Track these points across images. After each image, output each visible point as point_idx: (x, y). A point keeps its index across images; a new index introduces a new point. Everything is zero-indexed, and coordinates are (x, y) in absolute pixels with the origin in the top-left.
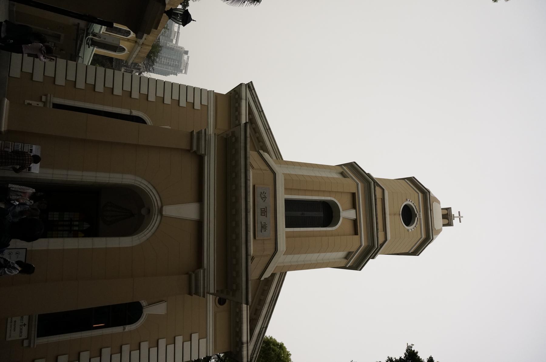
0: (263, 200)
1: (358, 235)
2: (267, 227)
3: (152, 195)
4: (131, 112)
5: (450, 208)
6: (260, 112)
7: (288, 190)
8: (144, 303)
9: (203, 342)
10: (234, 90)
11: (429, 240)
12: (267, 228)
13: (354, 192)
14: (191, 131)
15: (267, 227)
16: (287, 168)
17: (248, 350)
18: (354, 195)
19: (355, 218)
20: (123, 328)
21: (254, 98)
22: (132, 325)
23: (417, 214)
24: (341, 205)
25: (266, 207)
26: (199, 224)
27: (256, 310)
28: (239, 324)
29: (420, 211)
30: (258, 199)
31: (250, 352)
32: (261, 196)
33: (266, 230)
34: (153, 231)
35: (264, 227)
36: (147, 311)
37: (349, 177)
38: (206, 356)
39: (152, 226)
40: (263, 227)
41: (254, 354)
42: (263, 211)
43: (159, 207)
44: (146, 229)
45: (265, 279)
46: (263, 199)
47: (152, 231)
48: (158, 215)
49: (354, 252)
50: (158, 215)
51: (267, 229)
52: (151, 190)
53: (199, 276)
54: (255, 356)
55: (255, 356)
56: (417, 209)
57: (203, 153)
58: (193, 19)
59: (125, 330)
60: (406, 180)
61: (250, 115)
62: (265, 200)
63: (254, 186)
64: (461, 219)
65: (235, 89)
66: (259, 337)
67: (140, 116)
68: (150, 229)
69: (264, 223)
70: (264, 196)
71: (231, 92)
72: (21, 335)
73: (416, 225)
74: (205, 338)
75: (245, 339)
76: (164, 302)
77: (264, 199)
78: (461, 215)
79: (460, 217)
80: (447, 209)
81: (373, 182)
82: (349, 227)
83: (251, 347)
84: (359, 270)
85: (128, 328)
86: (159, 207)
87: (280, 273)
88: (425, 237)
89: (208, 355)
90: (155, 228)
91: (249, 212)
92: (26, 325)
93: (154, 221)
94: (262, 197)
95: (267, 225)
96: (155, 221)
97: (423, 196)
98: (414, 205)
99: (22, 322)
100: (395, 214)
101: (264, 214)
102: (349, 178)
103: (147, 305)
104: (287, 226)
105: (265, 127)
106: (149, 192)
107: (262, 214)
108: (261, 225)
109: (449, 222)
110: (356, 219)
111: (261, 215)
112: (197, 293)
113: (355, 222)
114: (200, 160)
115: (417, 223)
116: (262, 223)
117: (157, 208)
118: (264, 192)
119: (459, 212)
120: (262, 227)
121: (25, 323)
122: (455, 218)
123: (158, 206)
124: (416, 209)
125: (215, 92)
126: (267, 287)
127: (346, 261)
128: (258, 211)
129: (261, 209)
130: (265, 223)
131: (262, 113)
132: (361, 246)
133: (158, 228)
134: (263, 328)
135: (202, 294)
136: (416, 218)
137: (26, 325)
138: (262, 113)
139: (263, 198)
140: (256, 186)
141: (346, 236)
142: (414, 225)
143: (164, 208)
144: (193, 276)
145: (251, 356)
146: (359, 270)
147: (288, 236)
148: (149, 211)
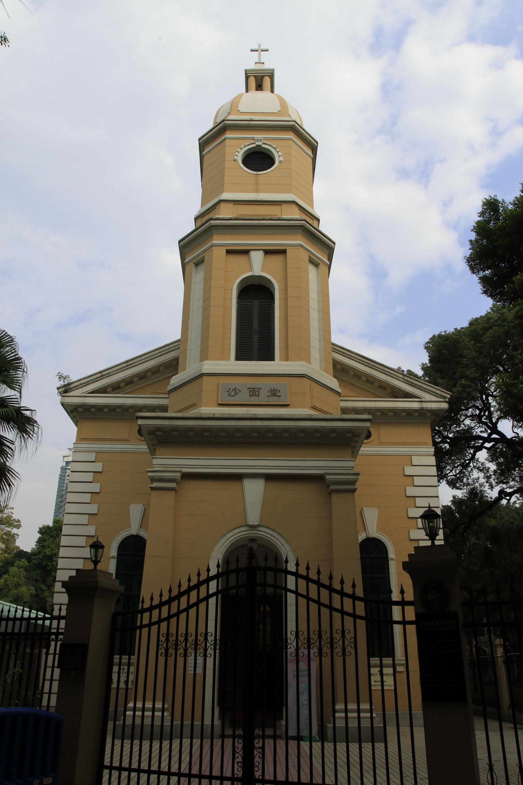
0: (238, 393)
1: (286, 250)
2: (274, 388)
3: (234, 537)
4: (113, 557)
5: (246, 71)
7: (224, 357)
8: (362, 537)
9: (415, 460)
11: (297, 128)
12: (272, 389)
15: (274, 388)
16: (191, 350)
17: (431, 402)
18: (229, 252)
20: (392, 561)
21: (81, 384)
22: (388, 551)
23: (257, 144)
24: (244, 273)
25: (248, 389)
26: (269, 478)
27: (380, 387)
28: (396, 412)
29: (253, 139)
30: (237, 400)
31: (434, 398)
32: (234, 396)
33: (278, 389)
35: (274, 393)
36: (373, 533)
38: (434, 456)
39: (272, 538)
40: (274, 394)
41: (436, 393)
44: (276, 544)
45: (340, 387)
46: (236, 393)
48: (258, 530)
49: (309, 256)
50: (258, 530)
51: (277, 389)
52: (228, 539)
54: (438, 392)
55: (438, 392)
56: (249, 143)
57: (179, 474)
58: (96, 539)
59: (395, 558)
60: (204, 153)
61: (107, 390)
62: (238, 389)
63: (221, 405)
64: (263, 48)
65: (69, 412)
66: (416, 385)
67: (117, 546)
68: (275, 540)
69: (269, 392)
70: (233, 391)
71: (72, 416)
73: (273, 147)
74: (411, 457)
75: (415, 405)
76: (362, 510)
77: (237, 391)
78: (256, 48)
79: (259, 50)
80: (247, 77)
82: (277, 260)
83: (427, 397)
84: (334, 246)
85: (391, 555)
86: (248, 529)
87: (333, 353)
88: (291, 133)
89: (433, 453)
90: (274, 534)
91: (256, 416)
92: (125, 669)
93: (265, 534)
95: (271, 389)
96: (264, 533)
97: (229, 129)
98: (244, 147)
99: (376, 675)
100: (257, 183)
101: (257, 392)
103: (365, 532)
105: (125, 368)
106: (230, 542)
107: (257, 394)
108: (272, 397)
109: (269, 76)
111: (258, 396)
112: (354, 483)
113: (268, 252)
114: (187, 476)
115: (270, 146)
116: (269, 394)
117: (249, 532)
118: (229, 392)
119: (251, 51)
120: (274, 395)
122: (262, 62)
123: (249, 530)
124: (249, 145)
125: (75, 442)
126: (350, 371)
127: (321, 266)
128: (254, 400)
129: (250, 396)
130: (269, 391)
131: (103, 373)
132: (302, 246)
134: (404, 379)
135: (355, 477)
136: (263, 146)
137: (125, 669)
138: (103, 373)
139: (235, 392)
140: (220, 402)
141: (288, 269)
142: (273, 151)
143: (250, 523)
144: (333, 487)
145: (438, 397)
146: (334, 246)
147: (286, 358)
148: (253, 540)
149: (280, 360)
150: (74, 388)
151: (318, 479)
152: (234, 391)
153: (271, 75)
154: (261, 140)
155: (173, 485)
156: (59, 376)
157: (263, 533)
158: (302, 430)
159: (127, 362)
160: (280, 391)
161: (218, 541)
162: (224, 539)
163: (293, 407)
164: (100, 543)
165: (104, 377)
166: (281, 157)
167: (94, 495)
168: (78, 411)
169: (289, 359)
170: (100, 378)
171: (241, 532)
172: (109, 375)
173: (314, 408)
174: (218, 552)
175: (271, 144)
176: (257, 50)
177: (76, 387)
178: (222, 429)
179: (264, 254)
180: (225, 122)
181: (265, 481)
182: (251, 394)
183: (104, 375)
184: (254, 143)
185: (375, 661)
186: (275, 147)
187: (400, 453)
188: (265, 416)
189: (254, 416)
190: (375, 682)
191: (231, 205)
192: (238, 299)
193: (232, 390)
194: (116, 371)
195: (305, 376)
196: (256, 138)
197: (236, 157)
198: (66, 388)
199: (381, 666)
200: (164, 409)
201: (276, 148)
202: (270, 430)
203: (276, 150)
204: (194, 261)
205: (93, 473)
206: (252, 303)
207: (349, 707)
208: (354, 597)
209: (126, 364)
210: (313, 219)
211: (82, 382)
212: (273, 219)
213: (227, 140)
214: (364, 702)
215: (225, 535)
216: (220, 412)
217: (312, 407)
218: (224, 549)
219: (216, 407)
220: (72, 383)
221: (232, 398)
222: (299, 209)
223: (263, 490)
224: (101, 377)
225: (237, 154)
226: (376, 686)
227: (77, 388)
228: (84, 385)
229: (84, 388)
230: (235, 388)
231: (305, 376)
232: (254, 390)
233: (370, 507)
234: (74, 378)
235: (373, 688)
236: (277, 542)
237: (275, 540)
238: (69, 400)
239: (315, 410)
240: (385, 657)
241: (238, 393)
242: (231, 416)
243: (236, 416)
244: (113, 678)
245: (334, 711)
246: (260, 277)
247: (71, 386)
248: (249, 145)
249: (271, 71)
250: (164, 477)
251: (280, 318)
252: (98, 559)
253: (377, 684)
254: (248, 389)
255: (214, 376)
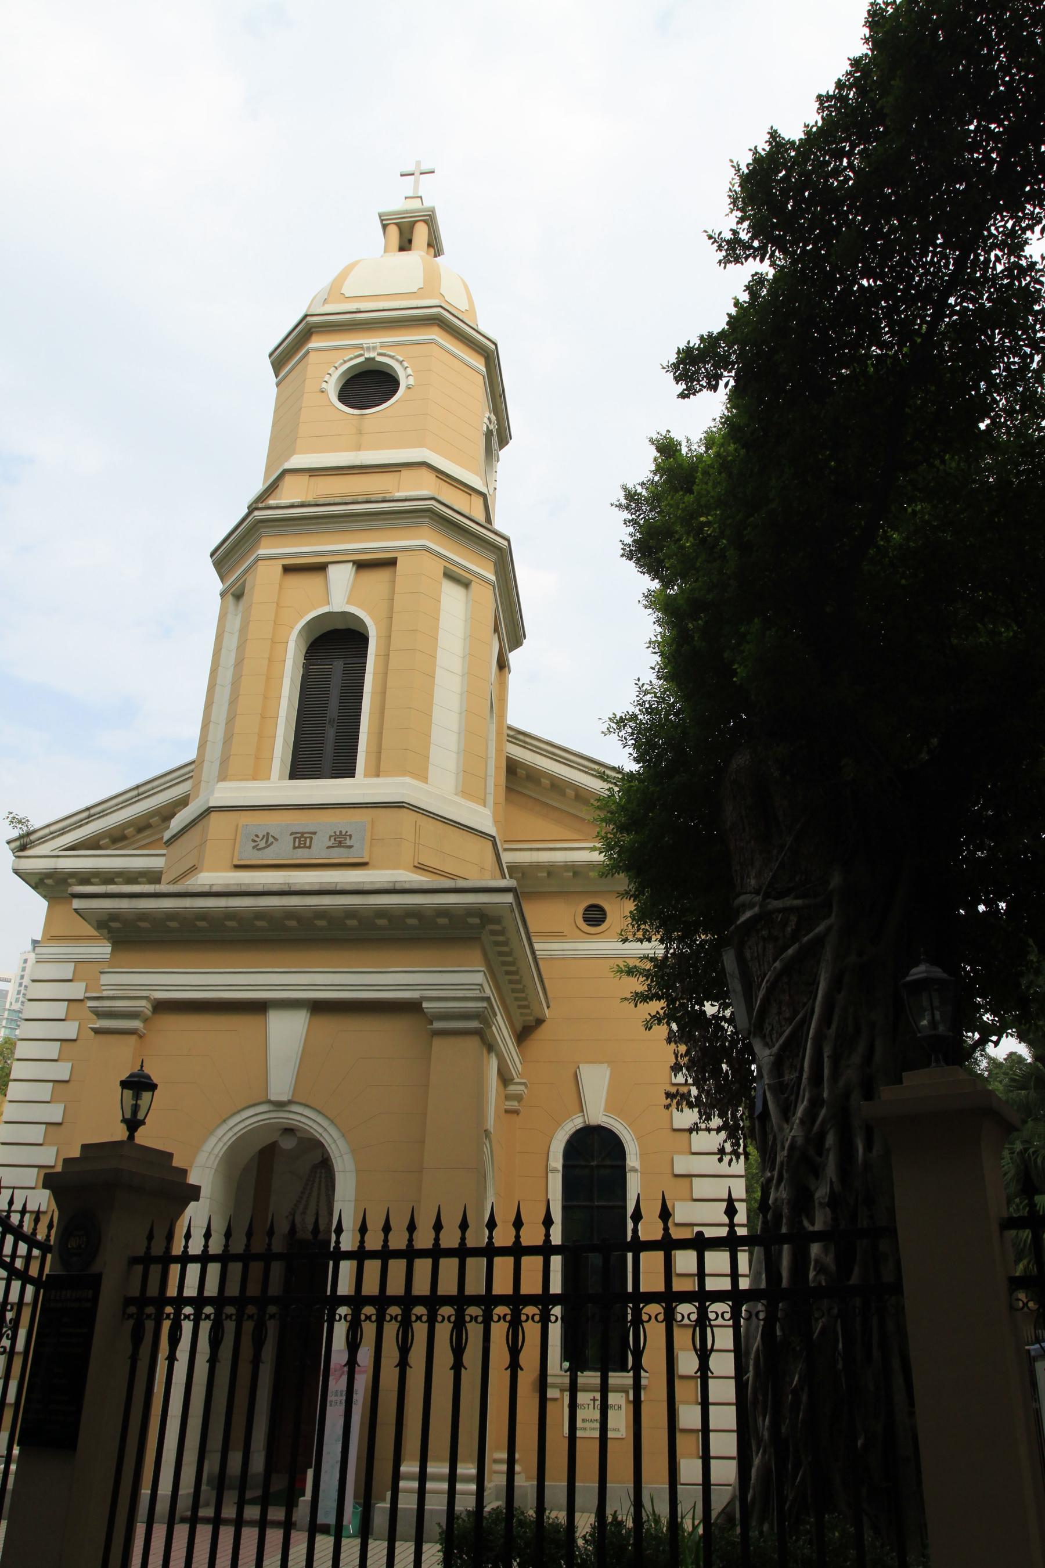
0: (272, 843)
2: (341, 832)
3: (242, 1125)
5: (379, 214)
6: (92, 816)
7: (258, 772)
10: (35, 887)
12: (344, 833)
13: (280, 569)
14: (93, 1033)
15: (341, 832)
18: (288, 569)
19: (351, 564)
21: (52, 833)
23: (367, 355)
26: (319, 1008)
29: (360, 347)
30: (269, 856)
34: (325, 1123)
35: (340, 840)
36: (597, 1115)
37: (241, 581)
39: (315, 1126)
42: (300, 843)
43: (272, 1108)
46: (269, 842)
47: (325, 1126)
50: (290, 1112)
51: (347, 832)
52: (231, 1129)
53: (443, 1010)
56: (352, 356)
63: (238, 867)
64: (424, 167)
68: (320, 1130)
69: (330, 840)
70: (262, 839)
72: (616, 1407)
73: (397, 360)
77: (271, 840)
79: (417, 173)
80: (385, 227)
81: (256, 513)
82: (378, 579)
85: (632, 1160)
88: (436, 329)
90: (319, 1119)
92: (594, 1397)
93: (303, 1119)
94: (264, 845)
95: (335, 832)
97: (317, 332)
98: (341, 364)
99: (586, 1406)
100: (360, 432)
101: (308, 840)
102: (245, 581)
103: (582, 1114)
104: (350, 773)
109: (425, 221)
110: (354, 562)
111: (310, 847)
113: (361, 566)
114: (163, 1007)
115: (392, 357)
116: (330, 844)
118: (254, 841)
119: (402, 175)
120: (340, 844)
121: (591, 1400)
123: (270, 1111)
124: (351, 359)
128: (302, 856)
129: (295, 848)
130: (331, 837)
131: (93, 811)
133: (319, 1112)
136: (379, 359)
137: (594, 1397)
138: (93, 811)
139: (267, 841)
141: (395, 595)
143: (273, 1098)
144: (438, 1025)
147: (376, 771)
149: (365, 776)
150: (38, 840)
151: (410, 1008)
152: (265, 838)
153: (430, 220)
154: (374, 348)
155: (136, 1024)
156: (9, 819)
157: (298, 1118)
158: (382, 912)
159: (137, 787)
160: (353, 837)
161: (212, 1133)
162: (225, 1127)
163: (375, 868)
164: (148, 1077)
165: (93, 818)
166: (409, 377)
167: (65, 1044)
168: (45, 884)
169: (381, 773)
170: (87, 820)
171: (256, 1115)
172: (102, 814)
173: (420, 868)
174: (210, 1153)
175: (392, 354)
176: (412, 172)
177: (42, 838)
178: (231, 915)
179: (354, 568)
180: (309, 319)
181: (309, 1014)
182: (297, 845)
183: (95, 815)
184: (361, 355)
185: (590, 1378)
186: (401, 359)
187: (82, 956)
188: (307, 888)
189: (286, 888)
190: (584, 1421)
191: (304, 478)
192: (305, 659)
193: (261, 837)
194: (116, 805)
195: (404, 804)
196: (365, 346)
197: (324, 385)
198: (22, 842)
199: (604, 1389)
200: (153, 876)
201: (403, 361)
202: (321, 914)
203: (403, 366)
204: (231, 592)
205: (67, 1003)
206: (331, 665)
207: (430, 1470)
208: (32, 1242)
209: (135, 793)
210: (470, 495)
211: (53, 828)
212: (373, 500)
213: (311, 354)
214: (439, 1459)
215: (224, 1121)
216: (221, 882)
217: (415, 866)
218: (223, 1147)
219: (228, 871)
220: (35, 831)
221: (260, 852)
222: (437, 476)
223: (305, 1031)
224: (89, 818)
225: (327, 378)
226: (585, 1429)
227: (43, 840)
228: (56, 834)
229: (57, 840)
230: (268, 834)
231: (404, 804)
232: (302, 836)
233: (596, 1062)
234: (36, 823)
235: (579, 1434)
236: (325, 1135)
237: (320, 1130)
238: (29, 865)
239: (424, 872)
240: (615, 1371)
241: (272, 843)
242: (244, 889)
243: (252, 889)
244: (568, 1410)
245: (396, 1476)
246: (344, 614)
247: (33, 837)
248: (351, 359)
249: (429, 211)
250: (113, 1009)
251: (372, 693)
252: (140, 1116)
253: (587, 1425)
254: (292, 834)
255: (231, 812)
